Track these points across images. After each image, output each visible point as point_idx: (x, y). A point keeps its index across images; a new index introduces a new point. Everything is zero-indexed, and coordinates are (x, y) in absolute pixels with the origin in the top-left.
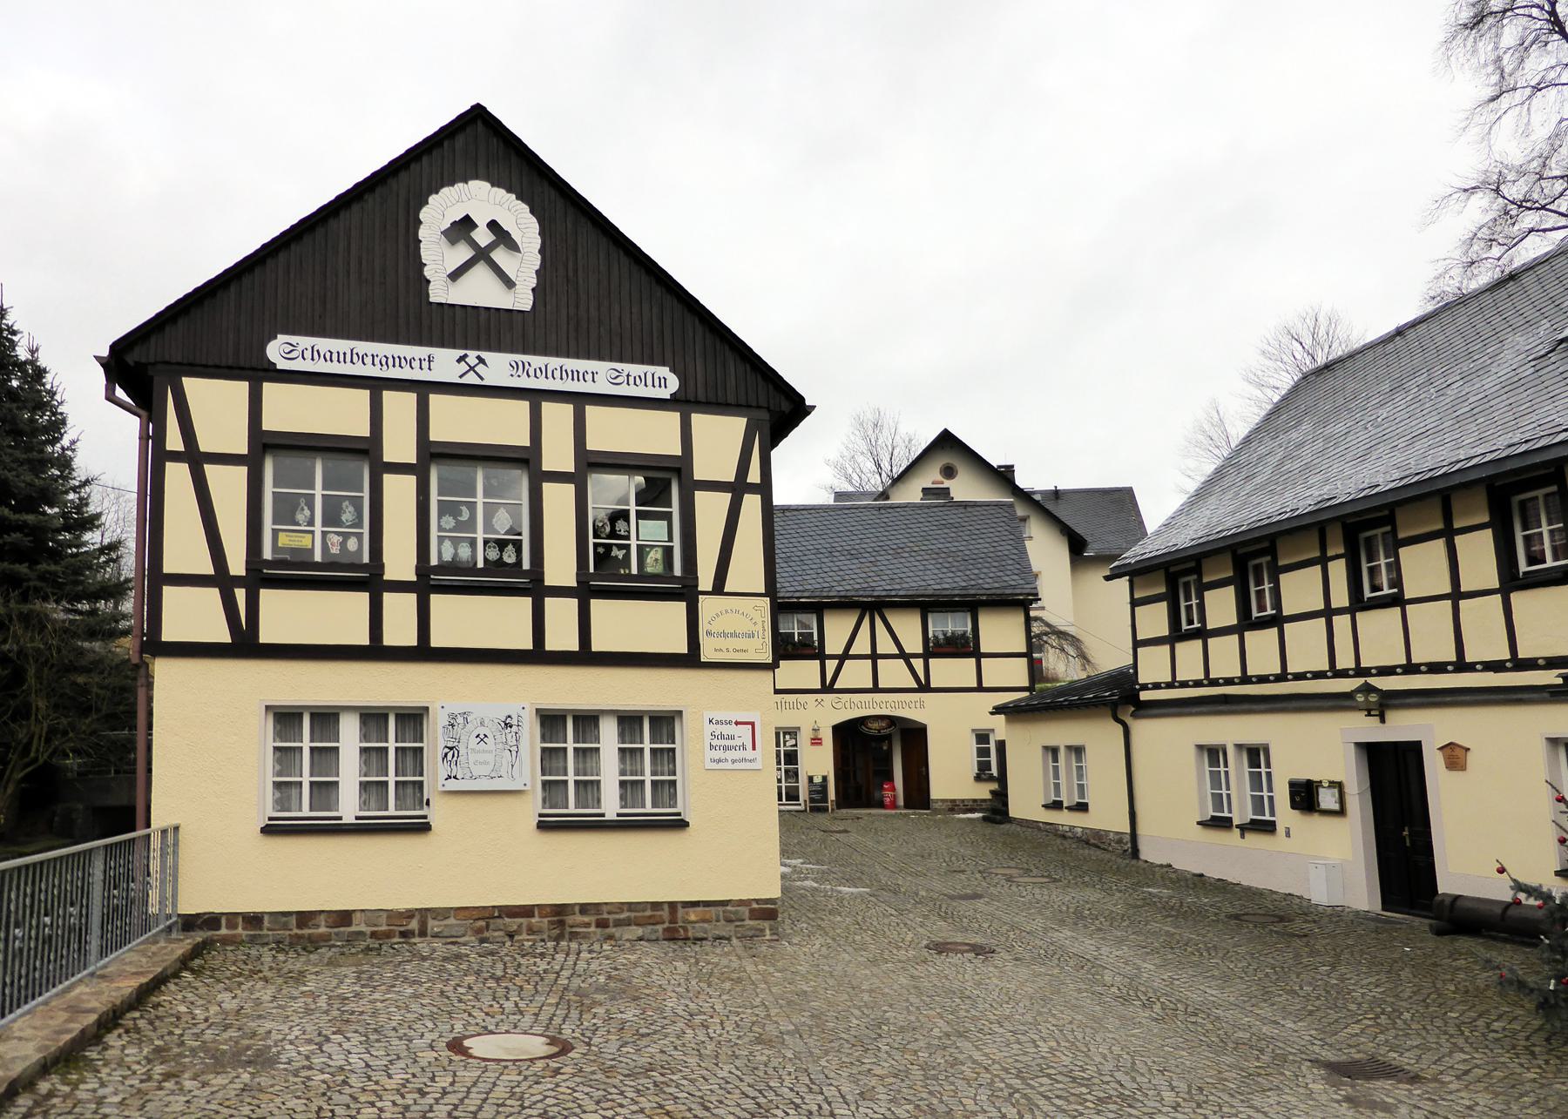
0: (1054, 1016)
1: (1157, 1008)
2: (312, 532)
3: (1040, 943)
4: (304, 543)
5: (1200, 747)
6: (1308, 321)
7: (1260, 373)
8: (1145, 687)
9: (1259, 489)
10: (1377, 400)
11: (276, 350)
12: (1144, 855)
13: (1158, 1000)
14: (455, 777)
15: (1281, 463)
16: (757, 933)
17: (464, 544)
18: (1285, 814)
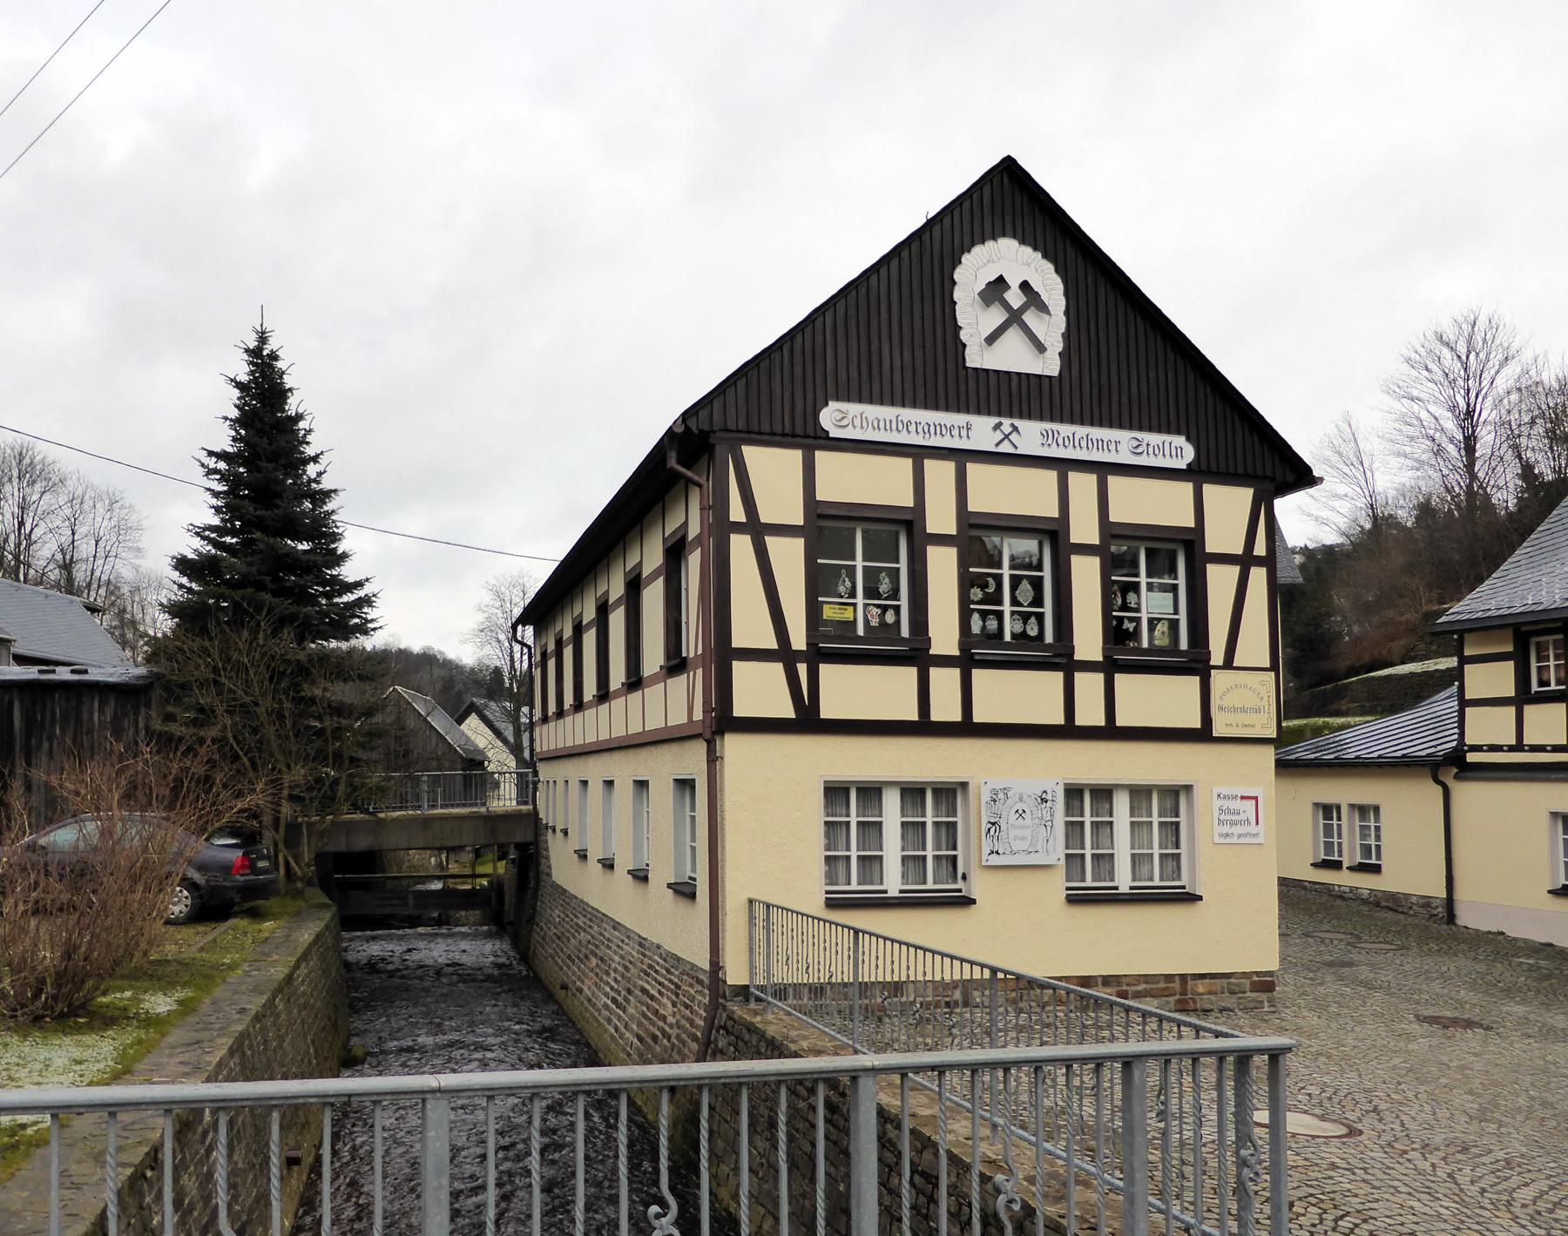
2: (854, 605)
4: (846, 616)
5: (1316, 805)
8: (1476, 748)
11: (836, 417)
12: (1460, 922)
14: (997, 852)
16: (1258, 1005)
17: (991, 617)
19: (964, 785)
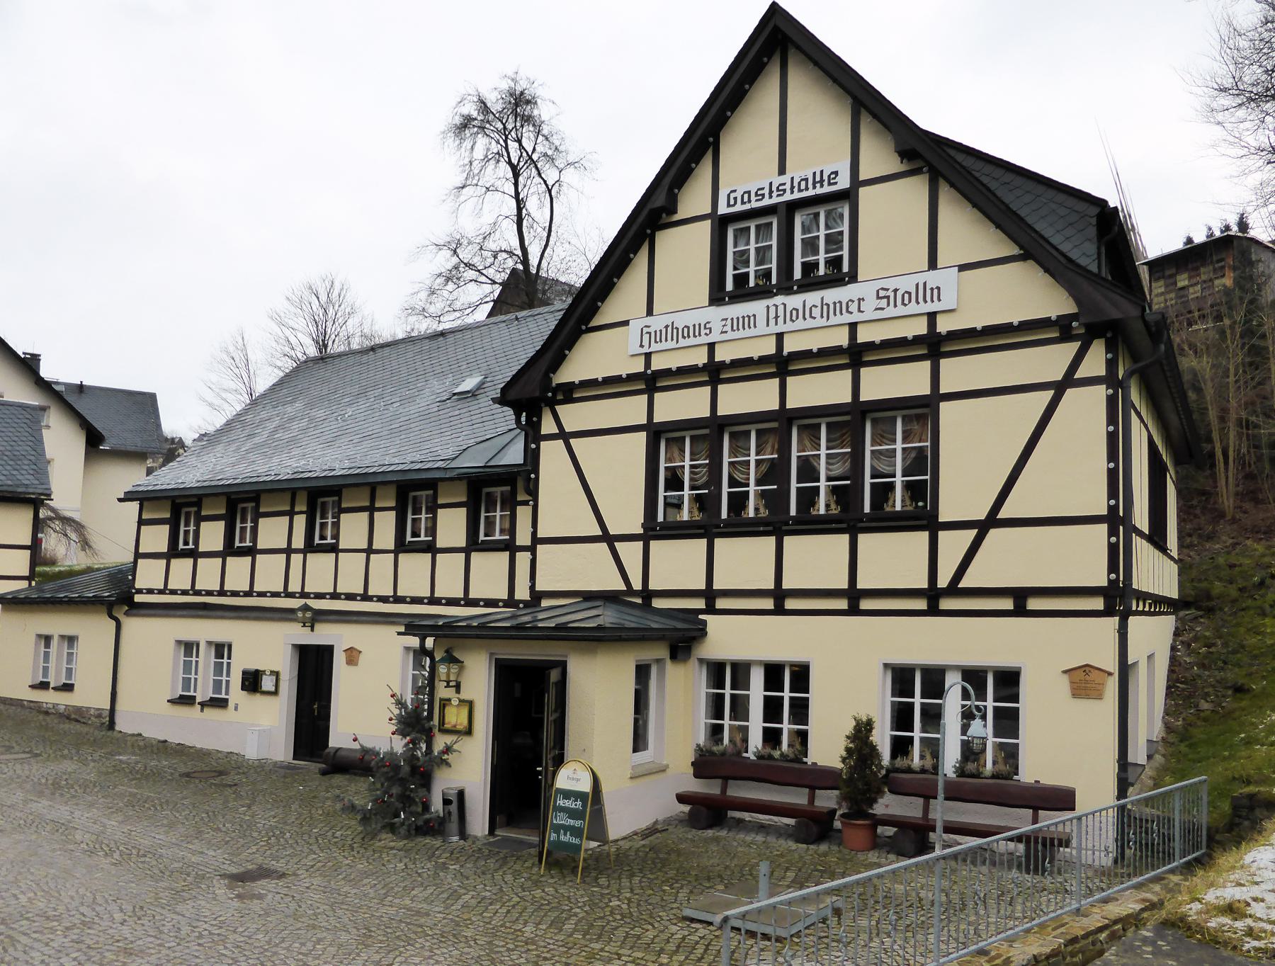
0: (32, 874)
1: (116, 855)
3: (18, 814)
5: (179, 642)
6: (326, 282)
7: (282, 315)
8: (140, 591)
9: (257, 447)
10: (348, 400)
12: (117, 728)
13: (118, 849)
15: (275, 431)
18: (236, 694)
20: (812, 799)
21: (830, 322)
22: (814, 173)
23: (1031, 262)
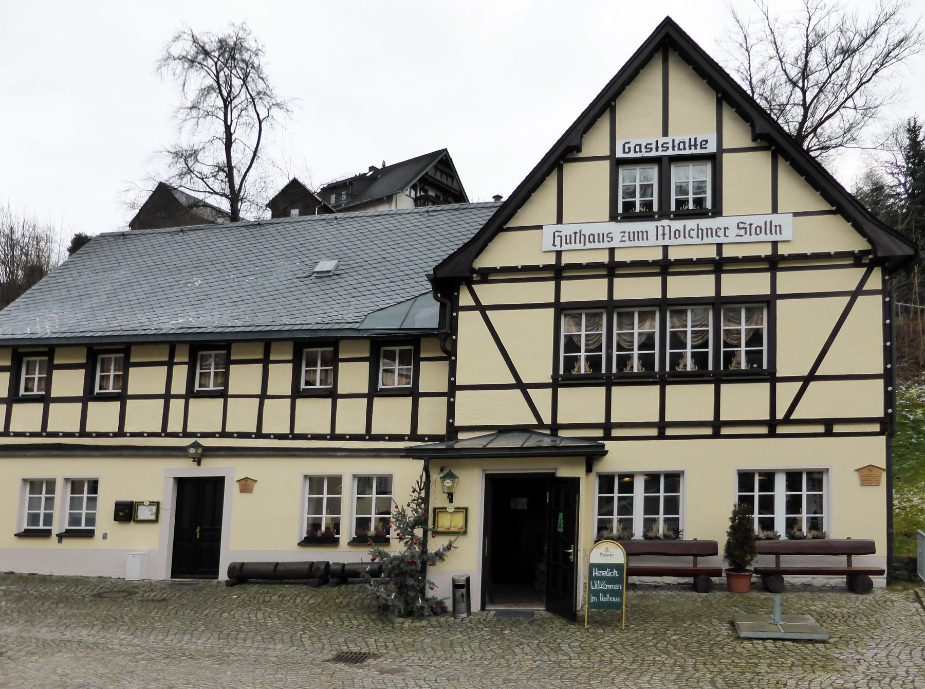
19: (827, 470)
20: (695, 563)
21: (704, 242)
22: (690, 139)
23: (839, 216)
